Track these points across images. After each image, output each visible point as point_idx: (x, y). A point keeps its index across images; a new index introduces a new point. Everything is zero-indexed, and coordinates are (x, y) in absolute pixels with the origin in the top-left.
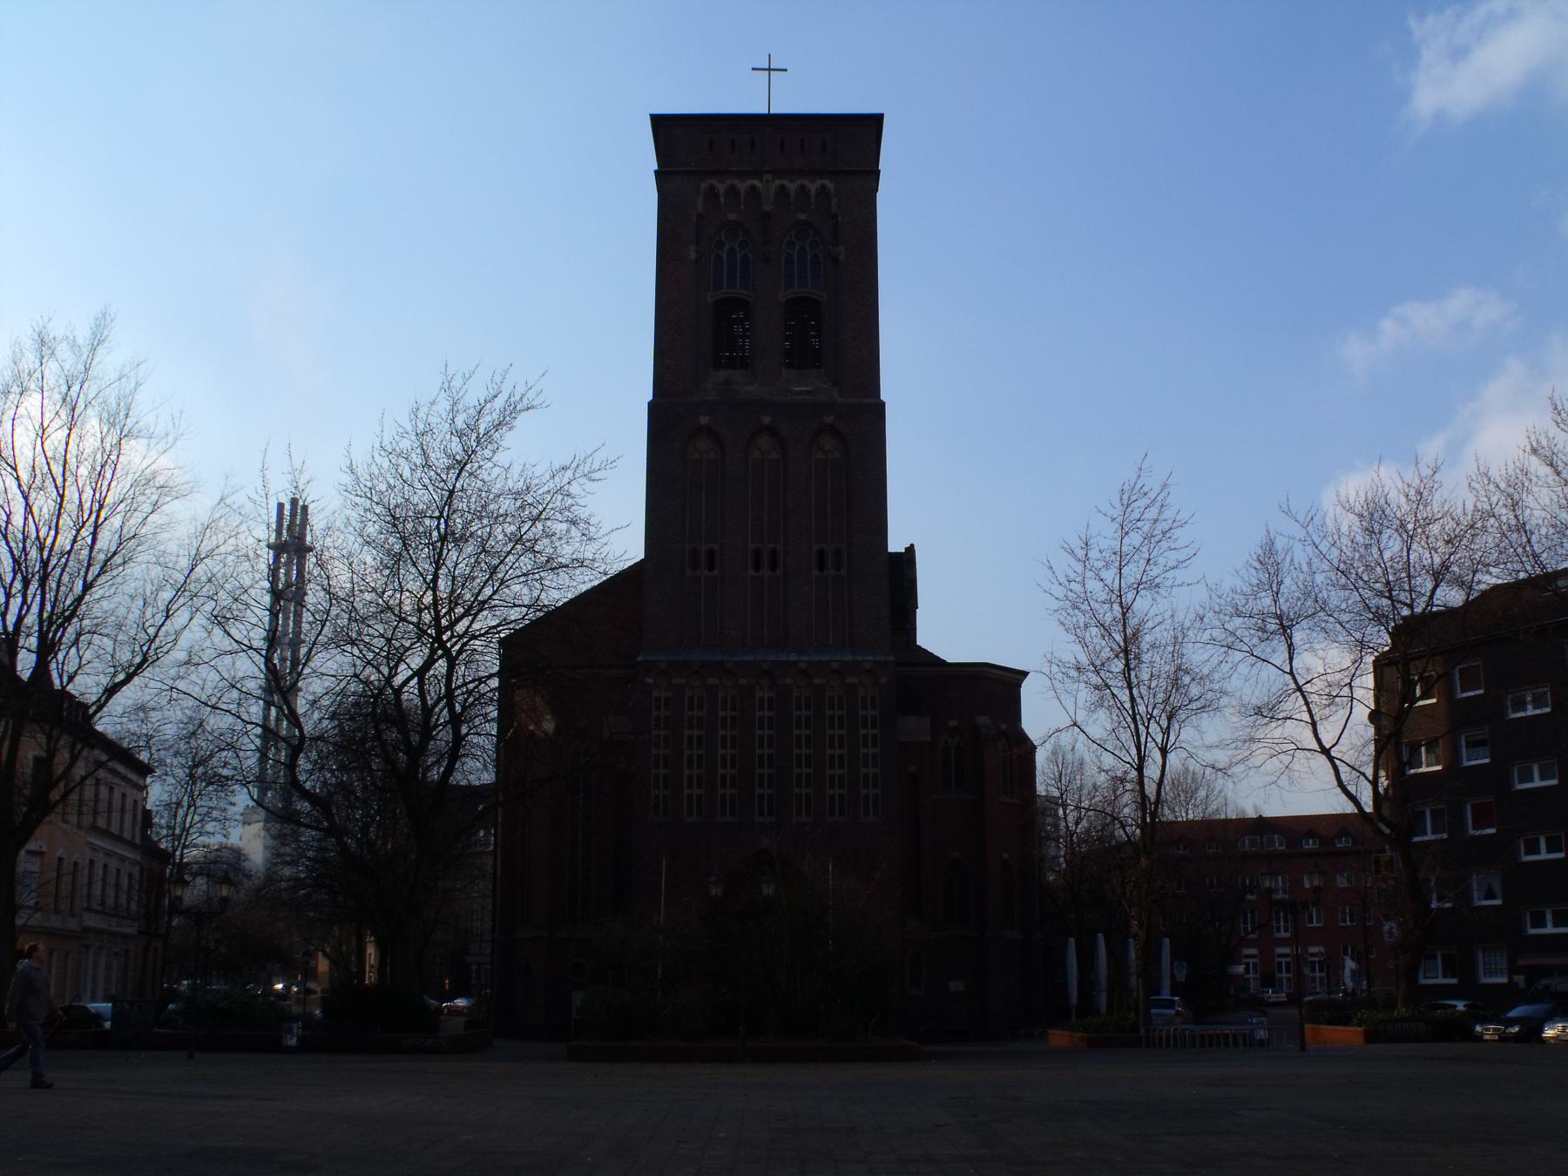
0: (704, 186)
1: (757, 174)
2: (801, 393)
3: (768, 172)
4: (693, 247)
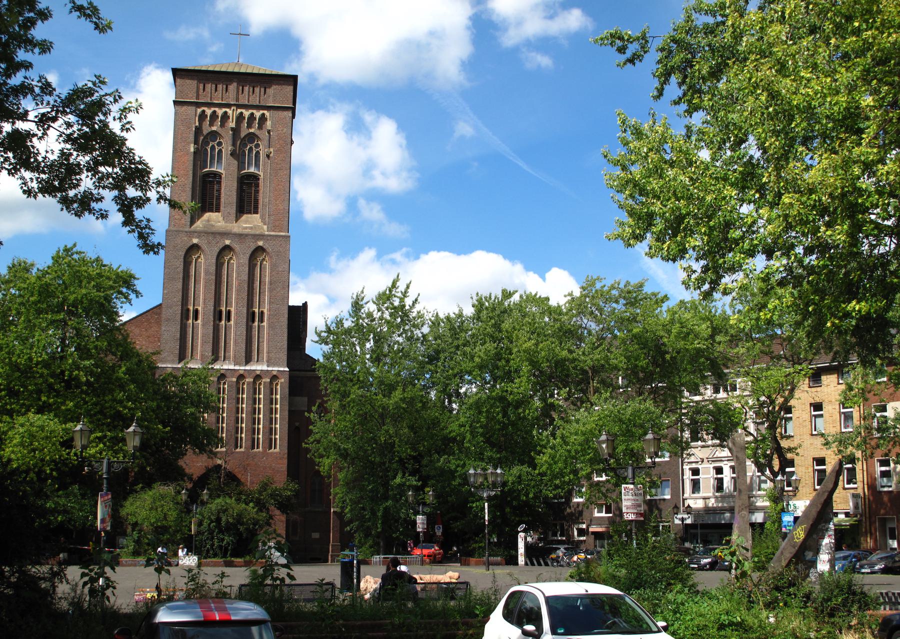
0: (199, 110)
1: (228, 106)
2: (246, 228)
4: (192, 145)
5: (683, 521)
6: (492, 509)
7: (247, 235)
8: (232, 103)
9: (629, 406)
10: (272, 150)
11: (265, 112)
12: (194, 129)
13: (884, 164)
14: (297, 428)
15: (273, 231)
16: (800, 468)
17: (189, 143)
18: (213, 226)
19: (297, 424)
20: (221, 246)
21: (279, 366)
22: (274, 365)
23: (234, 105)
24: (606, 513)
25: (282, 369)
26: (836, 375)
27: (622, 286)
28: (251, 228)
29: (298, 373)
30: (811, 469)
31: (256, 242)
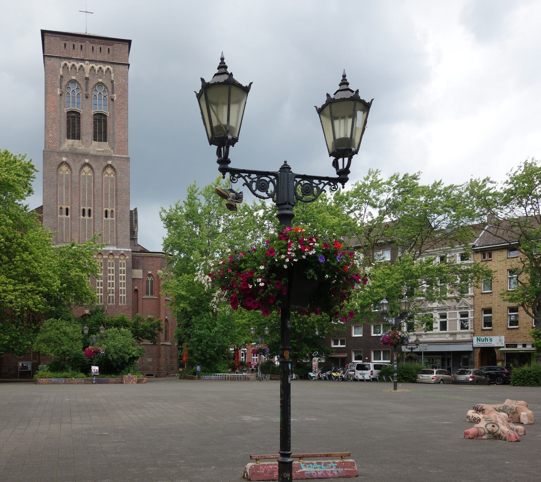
1: (83, 60)
2: (99, 151)
3: (88, 60)
4: (59, 89)
5: (412, 350)
6: (387, 358)
7: (100, 156)
8: (86, 59)
9: (514, 261)
10: (115, 95)
11: (110, 67)
12: (59, 77)
13: (211, 221)
14: (136, 290)
15: (118, 154)
16: (497, 315)
17: (56, 88)
18: (76, 149)
19: (136, 288)
20: (82, 163)
21: (124, 247)
22: (121, 247)
23: (88, 60)
24: (341, 344)
25: (127, 250)
26: (507, 251)
27: (400, 178)
28: (103, 151)
29: (136, 253)
30: (505, 315)
31: (106, 161)
